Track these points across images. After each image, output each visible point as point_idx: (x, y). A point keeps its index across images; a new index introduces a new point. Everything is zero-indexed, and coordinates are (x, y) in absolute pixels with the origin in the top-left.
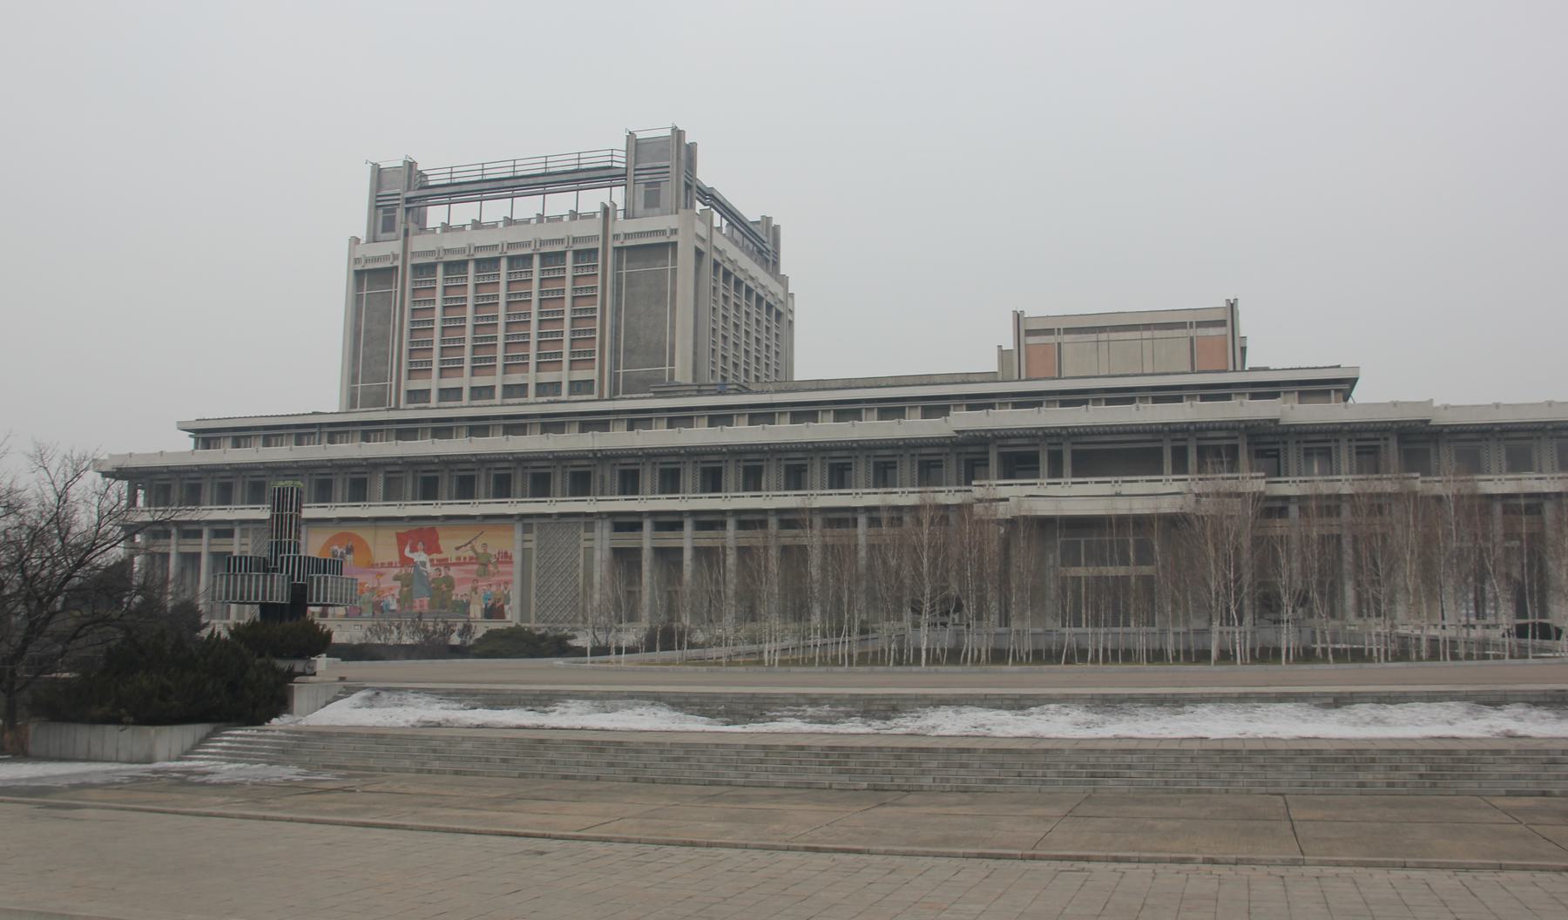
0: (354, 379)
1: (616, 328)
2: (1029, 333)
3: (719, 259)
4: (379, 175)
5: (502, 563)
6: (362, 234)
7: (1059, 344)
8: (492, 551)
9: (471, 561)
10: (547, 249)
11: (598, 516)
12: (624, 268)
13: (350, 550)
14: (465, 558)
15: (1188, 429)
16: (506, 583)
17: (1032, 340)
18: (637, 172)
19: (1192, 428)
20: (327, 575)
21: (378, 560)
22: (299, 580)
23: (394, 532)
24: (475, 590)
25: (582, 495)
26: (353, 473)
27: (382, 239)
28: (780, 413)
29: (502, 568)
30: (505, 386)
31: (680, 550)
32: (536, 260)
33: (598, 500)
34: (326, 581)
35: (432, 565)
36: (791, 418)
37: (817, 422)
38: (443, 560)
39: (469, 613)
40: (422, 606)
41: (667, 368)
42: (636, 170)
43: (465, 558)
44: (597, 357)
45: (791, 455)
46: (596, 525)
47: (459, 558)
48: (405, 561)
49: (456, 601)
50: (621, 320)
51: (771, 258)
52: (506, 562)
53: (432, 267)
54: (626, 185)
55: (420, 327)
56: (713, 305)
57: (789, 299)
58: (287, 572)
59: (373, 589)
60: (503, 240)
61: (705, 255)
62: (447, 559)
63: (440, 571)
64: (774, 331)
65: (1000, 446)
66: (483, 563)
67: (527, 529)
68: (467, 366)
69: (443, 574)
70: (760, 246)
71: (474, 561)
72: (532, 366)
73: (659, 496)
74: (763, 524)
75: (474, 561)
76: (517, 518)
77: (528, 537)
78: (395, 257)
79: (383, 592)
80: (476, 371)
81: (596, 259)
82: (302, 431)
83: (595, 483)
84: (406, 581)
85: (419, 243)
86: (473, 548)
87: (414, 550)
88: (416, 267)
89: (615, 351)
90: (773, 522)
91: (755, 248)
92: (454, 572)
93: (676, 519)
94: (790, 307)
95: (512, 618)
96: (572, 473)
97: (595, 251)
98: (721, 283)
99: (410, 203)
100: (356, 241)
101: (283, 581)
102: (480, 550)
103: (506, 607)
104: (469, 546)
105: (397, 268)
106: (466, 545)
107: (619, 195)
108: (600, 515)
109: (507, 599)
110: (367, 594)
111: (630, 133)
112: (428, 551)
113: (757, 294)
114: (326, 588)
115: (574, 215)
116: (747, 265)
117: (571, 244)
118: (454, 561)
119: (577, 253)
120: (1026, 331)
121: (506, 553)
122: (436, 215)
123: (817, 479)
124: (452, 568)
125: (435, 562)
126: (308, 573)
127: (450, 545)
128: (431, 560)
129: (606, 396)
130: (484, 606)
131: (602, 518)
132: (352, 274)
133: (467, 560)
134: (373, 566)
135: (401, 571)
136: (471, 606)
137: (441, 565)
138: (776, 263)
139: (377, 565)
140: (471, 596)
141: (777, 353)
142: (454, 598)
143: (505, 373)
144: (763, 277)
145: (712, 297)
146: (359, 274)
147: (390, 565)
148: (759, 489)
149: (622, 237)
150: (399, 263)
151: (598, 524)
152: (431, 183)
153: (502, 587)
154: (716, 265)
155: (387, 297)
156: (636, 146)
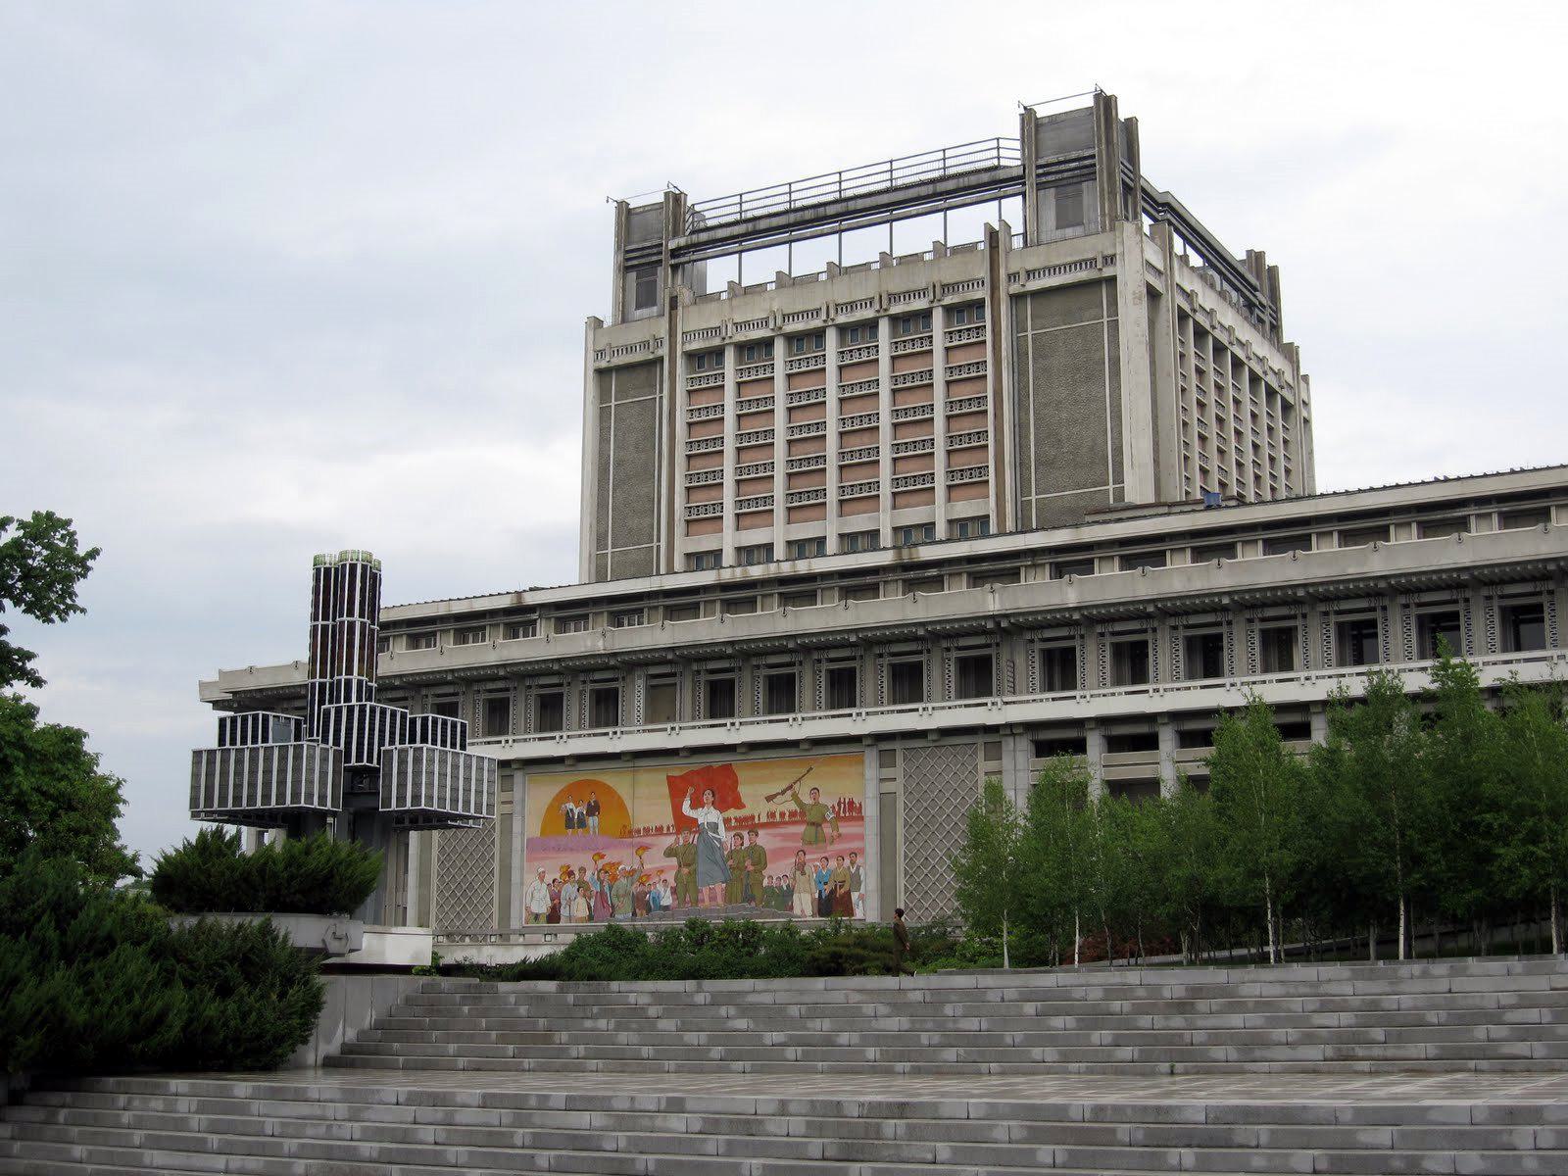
0: (600, 541)
1: (1020, 428)
3: (1186, 307)
4: (626, 216)
5: (845, 819)
6: (606, 312)
8: (828, 800)
9: (795, 818)
11: (1008, 732)
12: (1029, 329)
13: (593, 810)
14: (782, 815)
16: (854, 854)
20: (418, 745)
21: (639, 824)
22: (359, 758)
23: (664, 777)
24: (800, 867)
25: (977, 696)
26: (595, 681)
29: (845, 829)
33: (1007, 703)
34: (417, 760)
35: (728, 829)
36: (1339, 539)
37: (1388, 540)
38: (746, 819)
39: (792, 908)
40: (713, 898)
41: (1111, 487)
42: (1038, 167)
43: (782, 815)
46: (1004, 748)
47: (773, 815)
48: (683, 823)
49: (770, 887)
50: (1028, 414)
51: (1266, 318)
52: (851, 819)
54: (1024, 194)
55: (704, 452)
56: (1182, 417)
57: (1302, 384)
58: (336, 742)
59: (633, 872)
61: (1164, 298)
62: (753, 817)
63: (742, 838)
64: (1281, 434)
66: (810, 818)
67: (886, 759)
68: (779, 507)
69: (747, 844)
70: (1251, 297)
71: (798, 818)
72: (885, 499)
73: (1112, 691)
75: (798, 818)
76: (869, 741)
77: (888, 772)
79: (648, 876)
81: (982, 317)
82: (518, 617)
83: (1000, 670)
84: (685, 857)
85: (694, 320)
86: (795, 797)
87: (697, 804)
88: (690, 356)
89: (1021, 465)
91: (1242, 299)
92: (765, 839)
93: (1143, 729)
94: (1304, 396)
95: (867, 910)
97: (979, 304)
98: (1193, 349)
99: (678, 256)
100: (596, 323)
101: (324, 760)
102: (807, 800)
103: (855, 896)
104: (789, 792)
105: (661, 360)
106: (783, 792)
107: (1013, 210)
108: (1010, 729)
109: (856, 881)
110: (624, 881)
111: (1025, 108)
112: (721, 805)
113: (1251, 371)
114: (417, 774)
115: (940, 248)
116: (1229, 318)
118: (764, 819)
119: (949, 310)
121: (851, 803)
122: (719, 273)
124: (761, 832)
125: (733, 823)
126: (381, 743)
127: (757, 792)
128: (727, 821)
129: (1010, 525)
130: (817, 896)
131: (1013, 735)
132: (591, 373)
133: (787, 818)
134: (629, 833)
135: (677, 841)
136: (795, 897)
137: (741, 827)
138: (1276, 328)
139: (639, 831)
140: (794, 879)
141: (1288, 471)
142: (765, 882)
144: (1260, 347)
145: (1181, 404)
146: (601, 373)
147: (659, 830)
148: (1290, 667)
149: (1023, 275)
150: (664, 351)
151: (1008, 744)
152: (710, 223)
153: (847, 862)
154: (1183, 316)
155: (648, 408)
156: (1032, 125)
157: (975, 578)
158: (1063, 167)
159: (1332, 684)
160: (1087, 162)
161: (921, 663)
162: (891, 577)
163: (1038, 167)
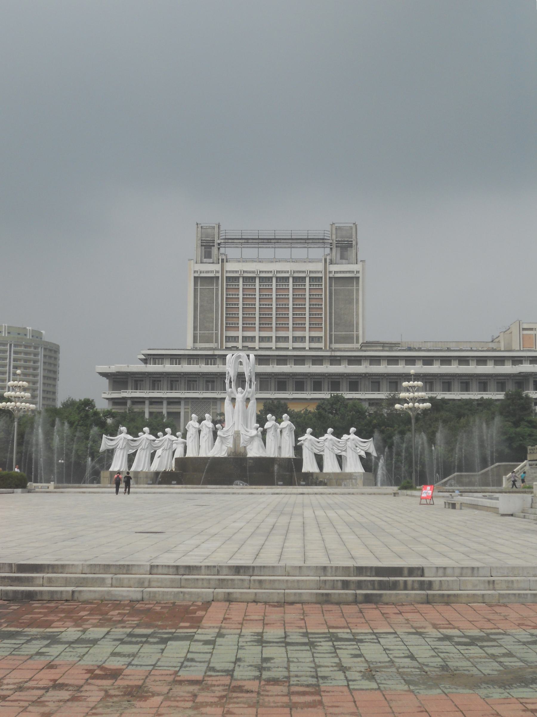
2: (524, 329)
7: (535, 334)
10: (296, 275)
15: (455, 376)
17: (525, 332)
18: (202, 241)
19: (291, 375)
27: (205, 262)
28: (272, 359)
30: (243, 337)
31: (179, 413)
32: (291, 280)
44: (323, 326)
45: (445, 378)
53: (236, 279)
60: (241, 269)
65: (534, 378)
74: (125, 404)
77: (187, 407)
78: (217, 272)
80: (245, 329)
81: (322, 282)
90: (147, 402)
96: (278, 381)
117: (275, 274)
120: (523, 328)
123: (309, 388)
143: (309, 331)
150: (219, 275)
157: (259, 359)
158: (343, 242)
159: (481, 396)
160: (350, 242)
161: (286, 381)
162: (327, 358)
163: (336, 241)
